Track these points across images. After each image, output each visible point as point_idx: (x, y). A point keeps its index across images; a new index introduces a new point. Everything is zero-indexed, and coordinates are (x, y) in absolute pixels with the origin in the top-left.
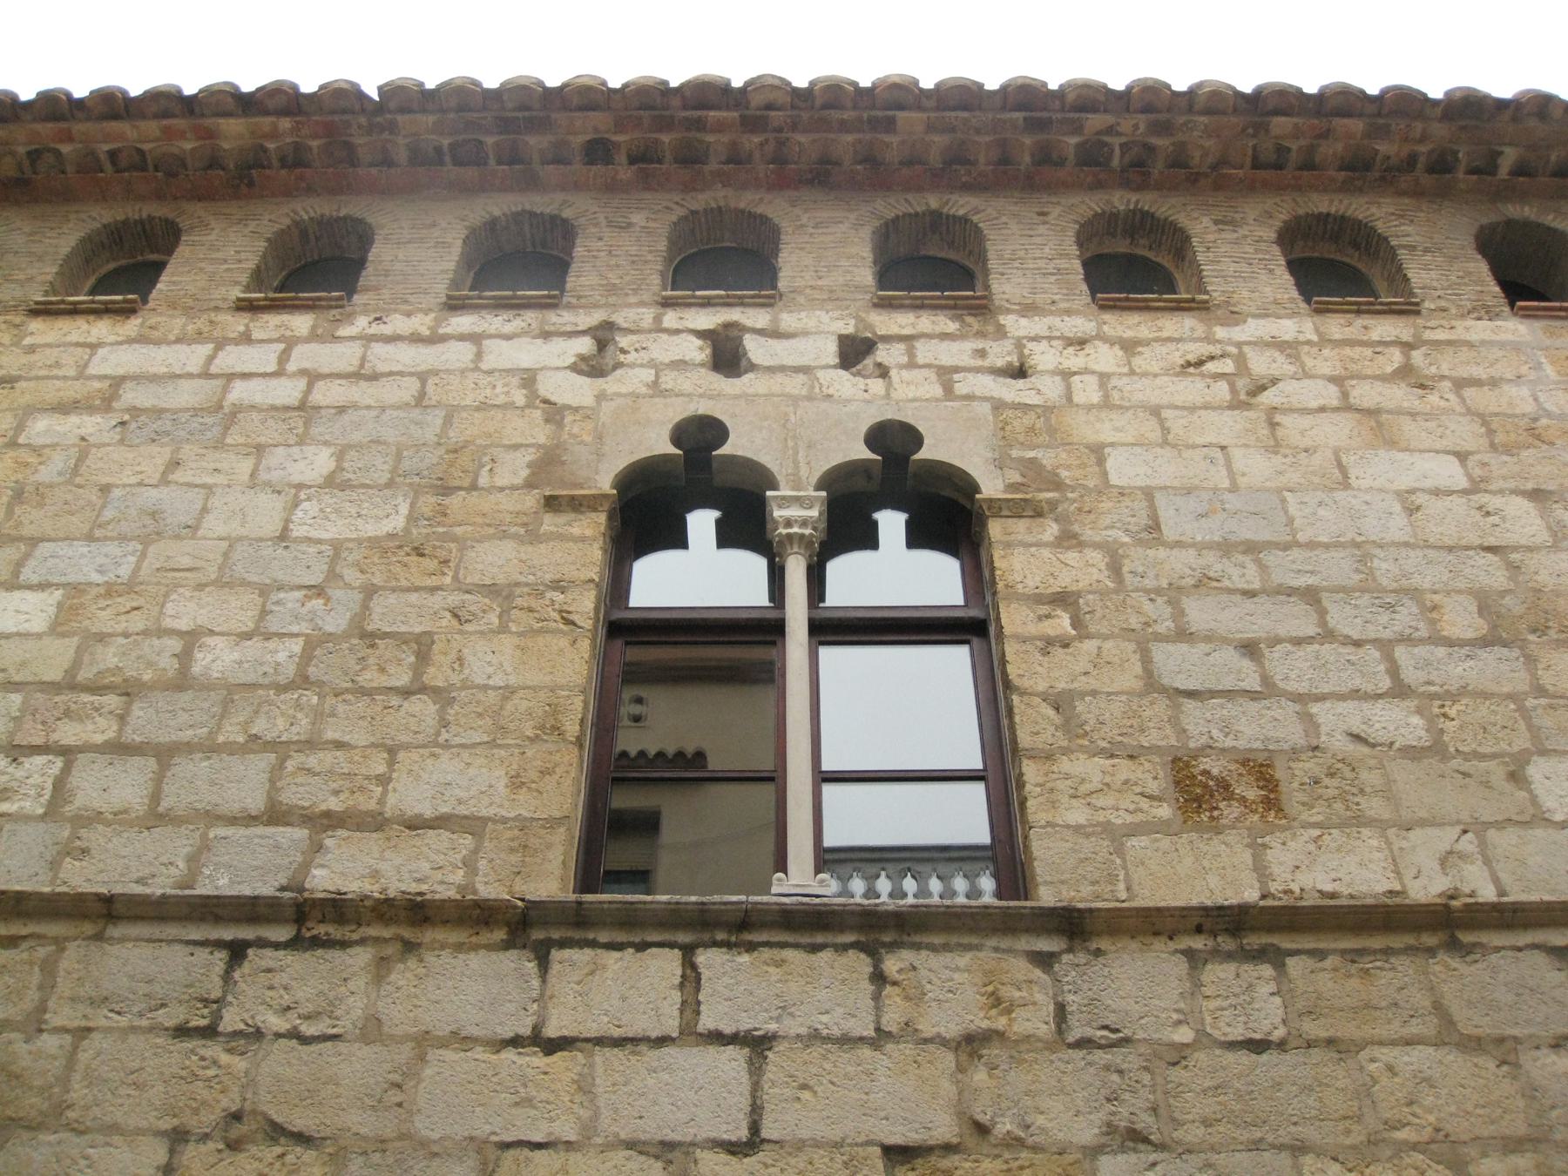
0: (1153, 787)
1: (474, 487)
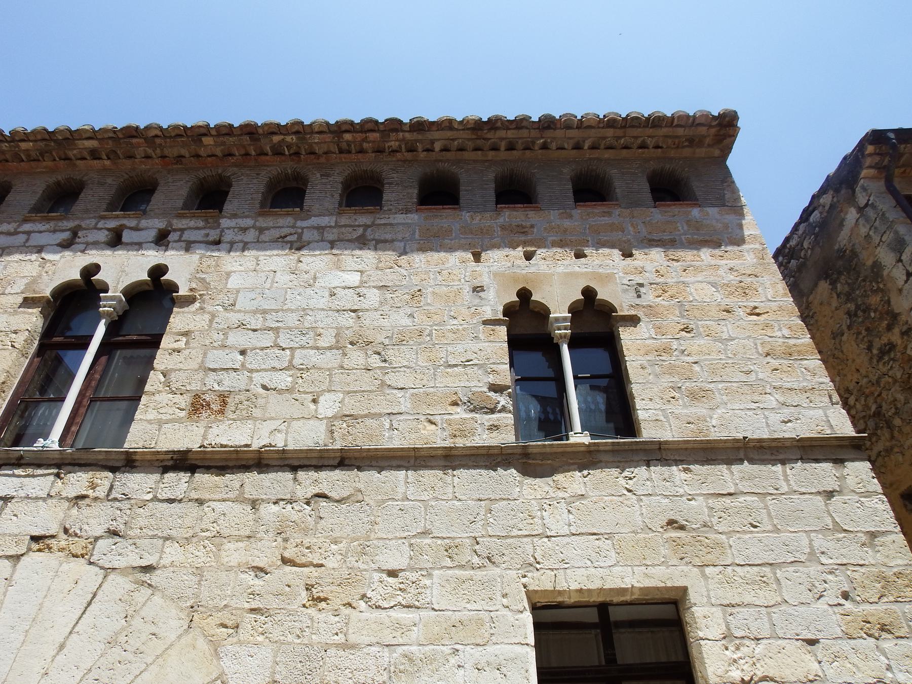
0: (183, 406)
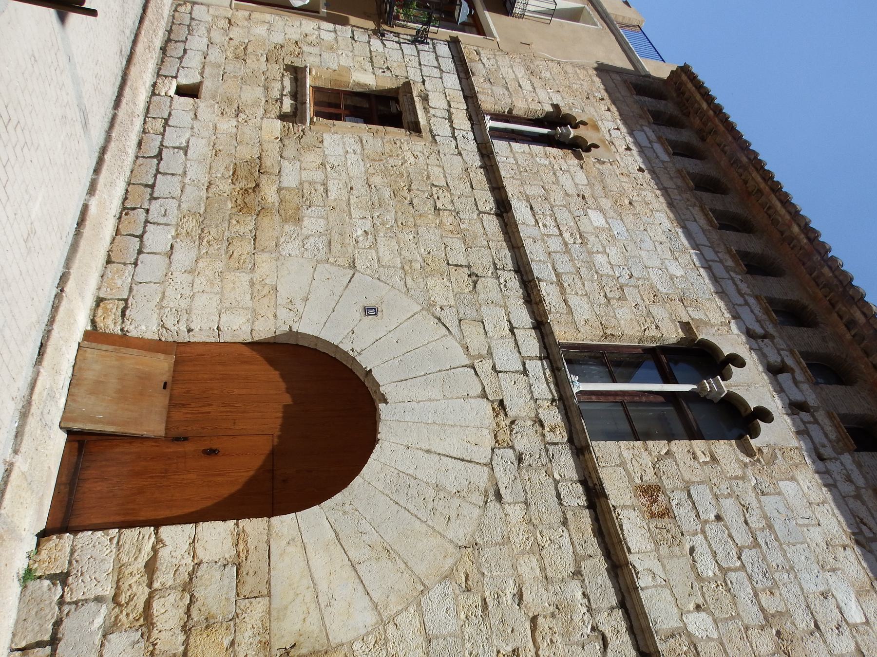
1: (685, 307)
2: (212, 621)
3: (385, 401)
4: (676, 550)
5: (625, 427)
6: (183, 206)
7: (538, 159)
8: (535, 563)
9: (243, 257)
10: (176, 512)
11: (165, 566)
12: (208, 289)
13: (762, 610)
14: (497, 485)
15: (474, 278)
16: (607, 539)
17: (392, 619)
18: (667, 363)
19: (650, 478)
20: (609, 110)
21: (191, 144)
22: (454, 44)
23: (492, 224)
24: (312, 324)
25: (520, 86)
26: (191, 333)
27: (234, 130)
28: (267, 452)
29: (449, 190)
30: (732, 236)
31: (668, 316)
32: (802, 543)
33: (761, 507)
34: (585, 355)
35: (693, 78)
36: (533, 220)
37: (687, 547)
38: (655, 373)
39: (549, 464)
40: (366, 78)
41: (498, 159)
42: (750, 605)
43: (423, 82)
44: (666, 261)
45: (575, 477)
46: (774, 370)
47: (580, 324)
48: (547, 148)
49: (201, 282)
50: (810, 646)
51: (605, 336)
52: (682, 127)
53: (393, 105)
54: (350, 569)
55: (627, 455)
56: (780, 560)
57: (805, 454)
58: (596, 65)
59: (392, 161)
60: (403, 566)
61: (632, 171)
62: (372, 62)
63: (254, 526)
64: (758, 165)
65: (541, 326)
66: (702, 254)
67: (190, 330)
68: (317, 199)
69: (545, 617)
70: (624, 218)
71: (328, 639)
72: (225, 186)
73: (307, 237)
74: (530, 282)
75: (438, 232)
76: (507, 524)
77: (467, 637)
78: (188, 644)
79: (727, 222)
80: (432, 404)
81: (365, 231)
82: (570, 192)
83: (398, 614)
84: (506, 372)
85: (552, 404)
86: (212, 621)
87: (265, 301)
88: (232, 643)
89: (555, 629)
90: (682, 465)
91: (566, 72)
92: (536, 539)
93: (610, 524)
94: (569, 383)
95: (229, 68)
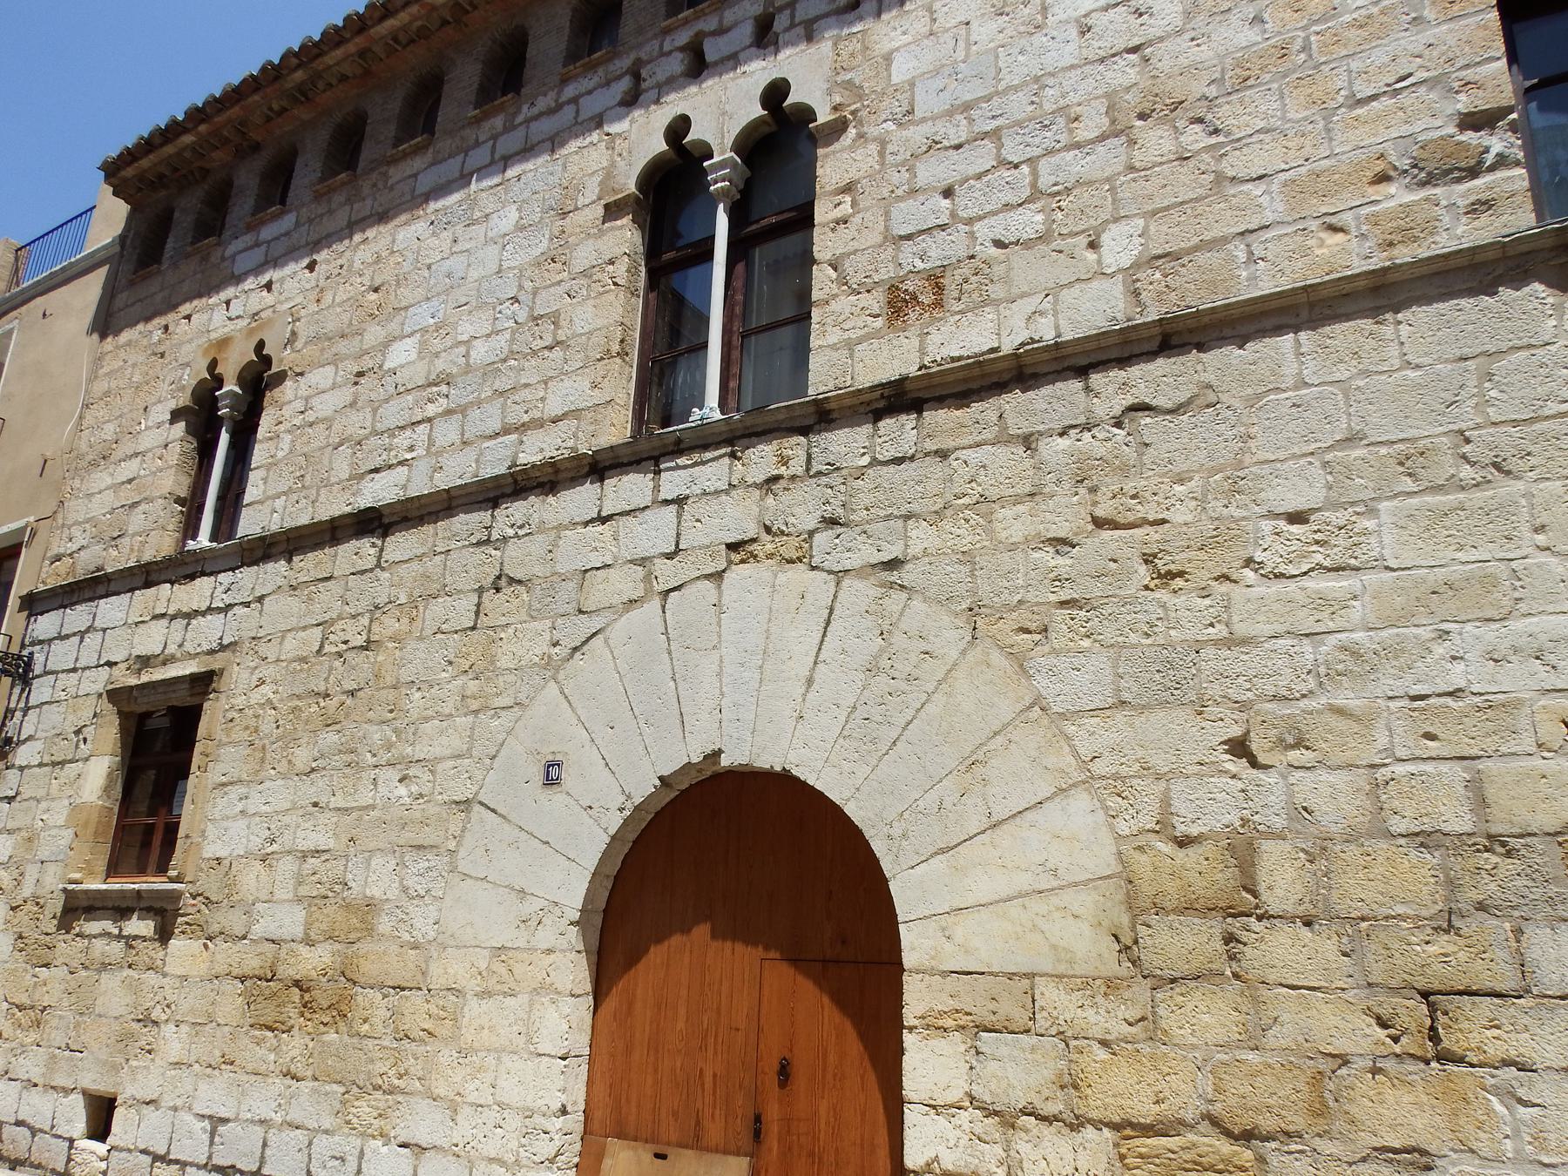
1: (577, 209)
2: (1067, 1079)
3: (717, 754)
4: (998, 270)
5: (786, 334)
6: (326, 1125)
7: (280, 454)
8: (1008, 512)
9: (434, 1010)
10: (882, 1138)
11: (970, 1159)
12: (489, 1077)
13: (1102, 138)
14: (873, 566)
15: (503, 582)
16: (975, 386)
17: (1084, 764)
18: (678, 250)
19: (875, 301)
20: (188, 317)
21: (207, 1112)
22: (34, 604)
23: (402, 544)
24: (570, 883)
25: (130, 481)
26: (569, 1109)
27: (184, 1028)
28: (792, 970)
29: (332, 622)
30: (447, 112)
31: (591, 241)
32: (997, 57)
33: (933, 119)
34: (656, 394)
35: (129, 156)
36: (400, 469)
37: (994, 251)
38: (694, 273)
39: (844, 472)
40: (96, 775)
41: (274, 528)
42: (1093, 157)
43: (110, 664)
44: (490, 234)
45: (867, 429)
46: (698, 67)
47: (598, 396)
48: (259, 436)
49: (475, 1091)
50: (1166, 65)
51: (623, 354)
52: (207, 192)
53: (153, 724)
54: (998, 831)
55: (834, 336)
56: (1022, 97)
57: (846, 31)
58: (95, 337)
59: (267, 727)
60: (999, 739)
61: (313, 283)
62: (62, 763)
63: (917, 998)
64: (309, 53)
65: (599, 467)
66: (478, 170)
67: (564, 1111)
68: (329, 870)
69: (1095, 503)
70: (403, 304)
71: (1108, 877)
72: (295, 1045)
73: (405, 890)
74: (516, 481)
75: (412, 644)
76: (939, 553)
77: (1120, 639)
78: (1101, 1122)
79: (421, 116)
80: (727, 669)
81: (400, 781)
82: (349, 399)
83: (1076, 754)
84: (678, 535)
85: (739, 459)
86: (1067, 1079)
87: (518, 969)
88: (1104, 1043)
89: (1116, 488)
90: (856, 245)
91: (107, 394)
92: (967, 506)
93: (951, 378)
94: (704, 426)
95: (59, 1038)
